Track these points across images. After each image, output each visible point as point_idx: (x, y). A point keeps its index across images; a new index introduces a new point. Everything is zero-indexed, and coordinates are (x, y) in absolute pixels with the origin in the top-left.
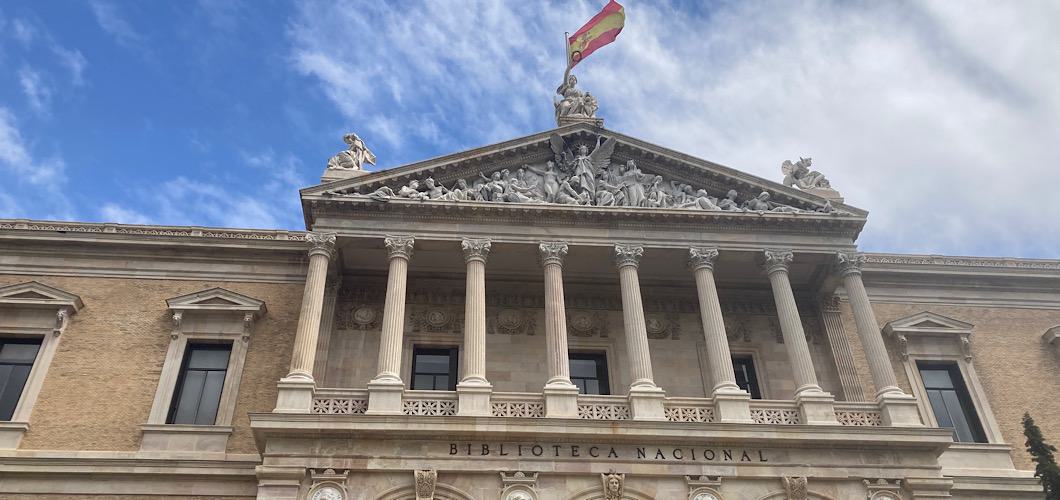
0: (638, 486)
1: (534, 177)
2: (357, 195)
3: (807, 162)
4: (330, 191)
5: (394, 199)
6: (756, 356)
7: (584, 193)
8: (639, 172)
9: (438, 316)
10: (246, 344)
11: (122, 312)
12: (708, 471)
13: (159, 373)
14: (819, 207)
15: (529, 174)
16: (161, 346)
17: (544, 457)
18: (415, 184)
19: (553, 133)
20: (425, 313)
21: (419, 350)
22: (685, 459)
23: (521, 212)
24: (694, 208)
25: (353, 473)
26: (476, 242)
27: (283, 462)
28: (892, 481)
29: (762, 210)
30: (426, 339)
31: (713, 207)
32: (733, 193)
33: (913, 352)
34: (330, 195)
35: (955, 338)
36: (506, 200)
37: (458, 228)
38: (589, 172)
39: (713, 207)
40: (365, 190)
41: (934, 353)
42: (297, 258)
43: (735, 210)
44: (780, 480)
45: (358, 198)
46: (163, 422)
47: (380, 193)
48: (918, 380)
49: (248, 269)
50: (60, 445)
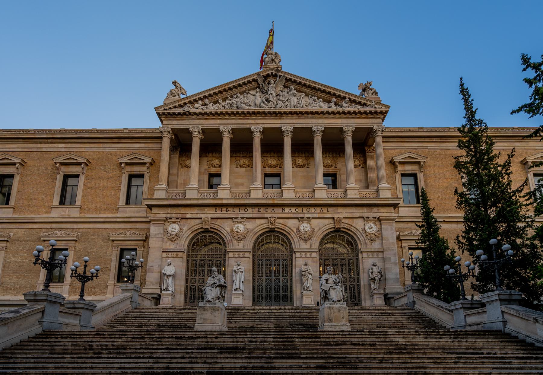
0: (281, 221)
1: (251, 96)
2: (177, 109)
3: (370, 84)
4: (166, 108)
5: (192, 110)
6: (338, 173)
7: (271, 103)
8: (295, 91)
9: (300, 160)
10: (149, 175)
11: (104, 165)
12: (307, 215)
13: (120, 187)
14: (369, 105)
15: (249, 95)
16: (120, 177)
17: (248, 212)
18: (200, 102)
19: (258, 74)
20: (212, 160)
21: (267, 175)
22: (299, 212)
23: (243, 113)
24: (316, 108)
25: (182, 218)
26: (226, 128)
27: (158, 215)
28: (375, 218)
29: (346, 107)
30: (269, 170)
31: (325, 107)
32: (334, 100)
33: (401, 169)
34: (166, 110)
35: (419, 163)
36: (237, 107)
37: (218, 122)
38: (273, 92)
39: (325, 107)
40: (181, 106)
41: (409, 169)
42: (159, 139)
43: (334, 108)
44: (333, 218)
45: (177, 110)
46: (124, 204)
47: (186, 108)
48: (400, 181)
49: (146, 145)
50: (92, 212)
